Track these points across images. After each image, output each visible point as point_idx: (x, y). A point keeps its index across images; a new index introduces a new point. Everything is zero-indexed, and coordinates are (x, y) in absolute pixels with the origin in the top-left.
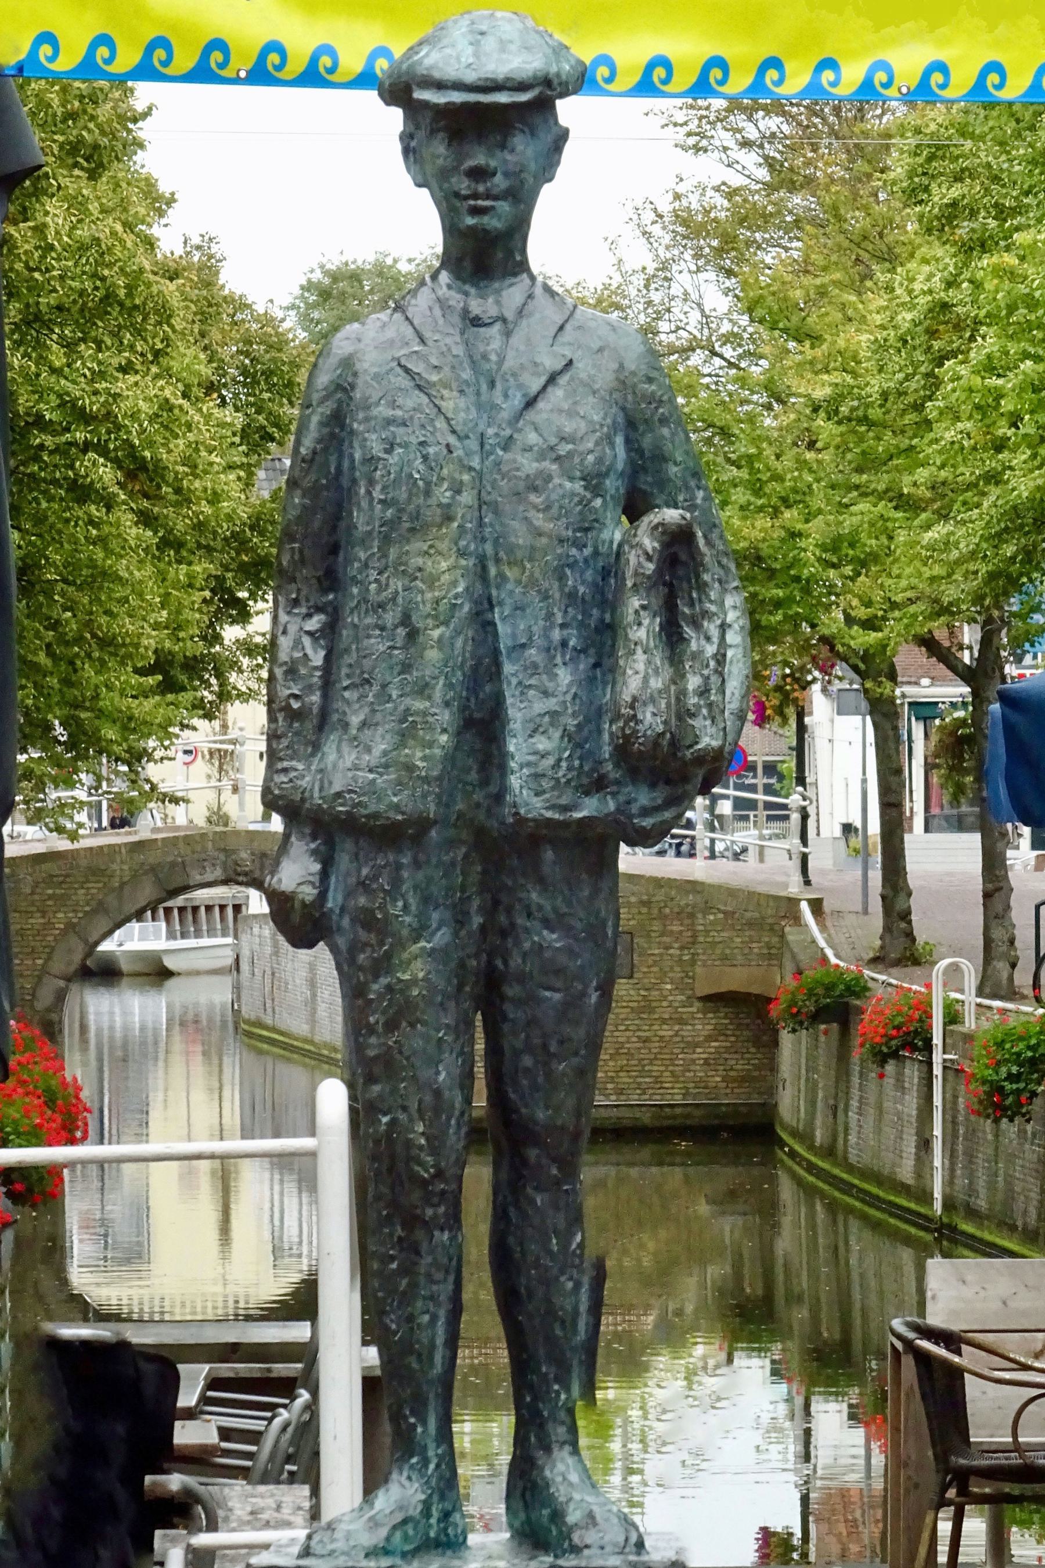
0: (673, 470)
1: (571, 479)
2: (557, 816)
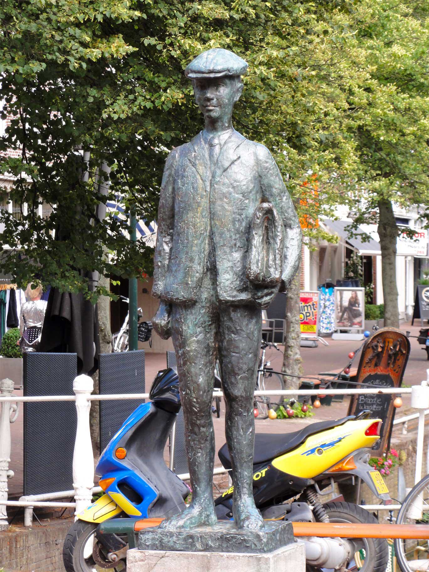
0: (274, 190)
1: (237, 194)
2: (231, 299)
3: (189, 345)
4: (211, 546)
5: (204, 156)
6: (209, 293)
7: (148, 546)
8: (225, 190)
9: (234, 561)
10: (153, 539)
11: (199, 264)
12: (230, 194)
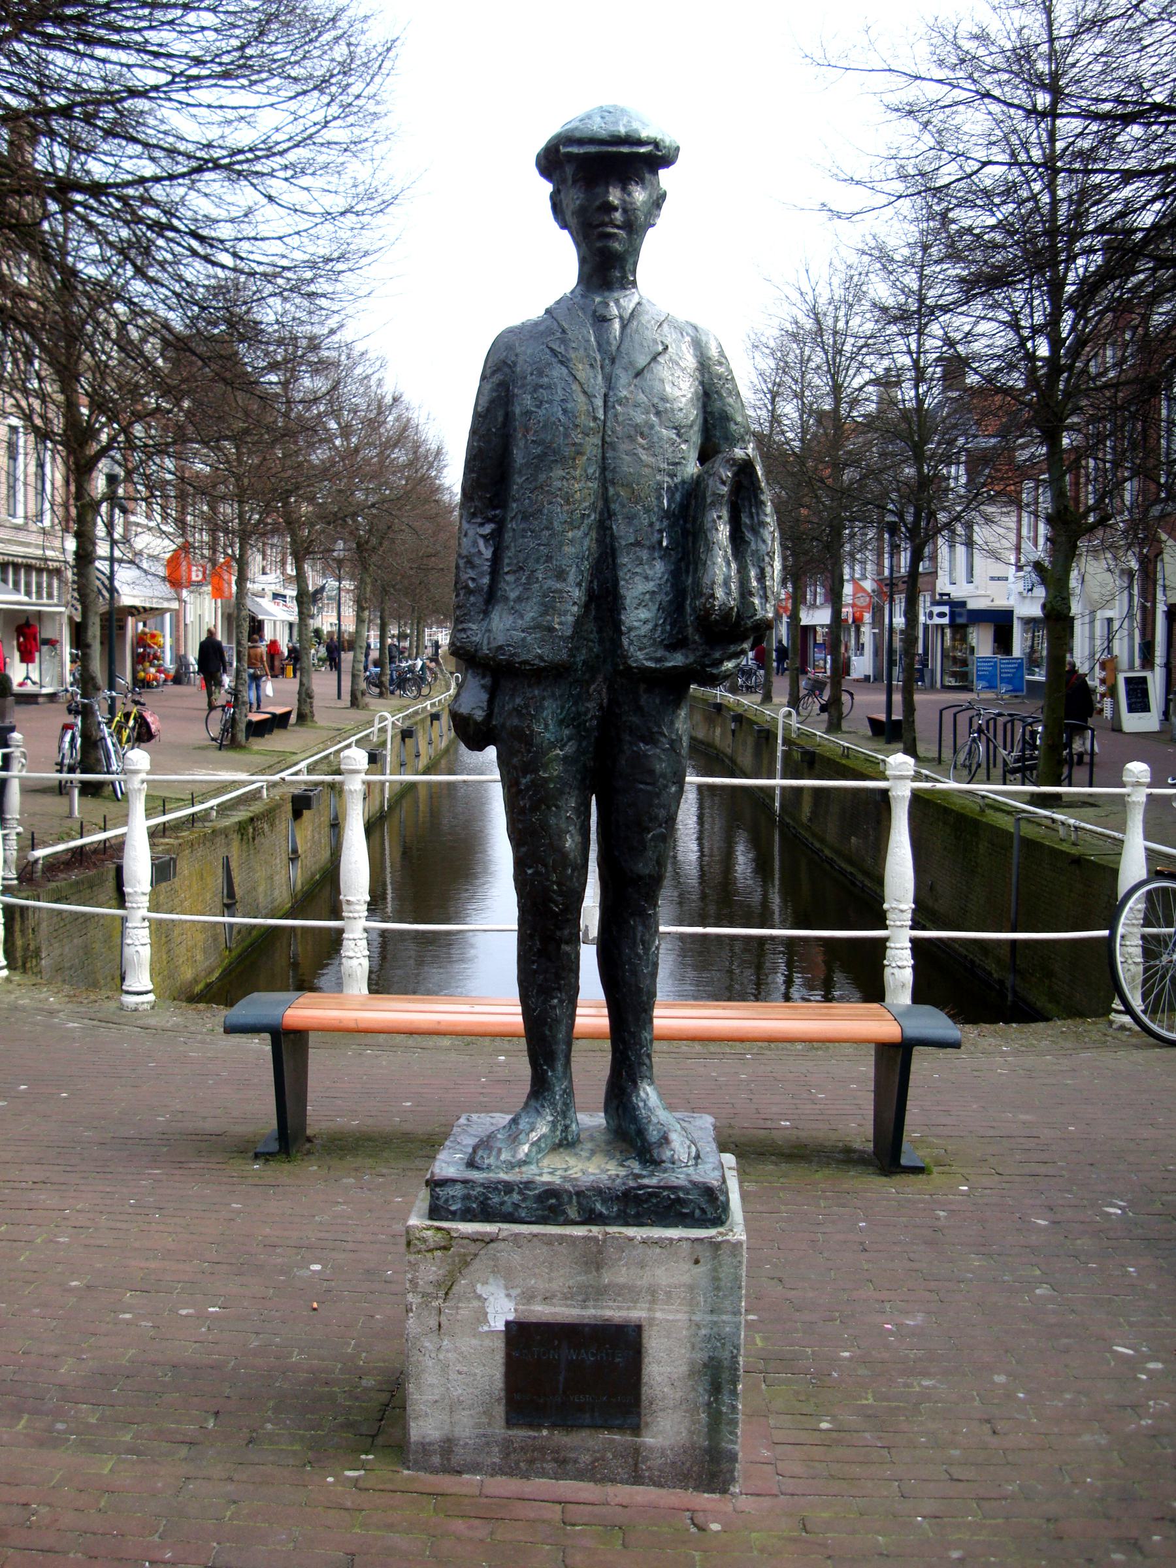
1: (667, 428)
3: (545, 767)
4: (601, 1214)
5: (588, 341)
6: (591, 649)
7: (454, 1213)
8: (640, 418)
9: (658, 1250)
10: (466, 1197)
11: (579, 585)
12: (652, 427)
